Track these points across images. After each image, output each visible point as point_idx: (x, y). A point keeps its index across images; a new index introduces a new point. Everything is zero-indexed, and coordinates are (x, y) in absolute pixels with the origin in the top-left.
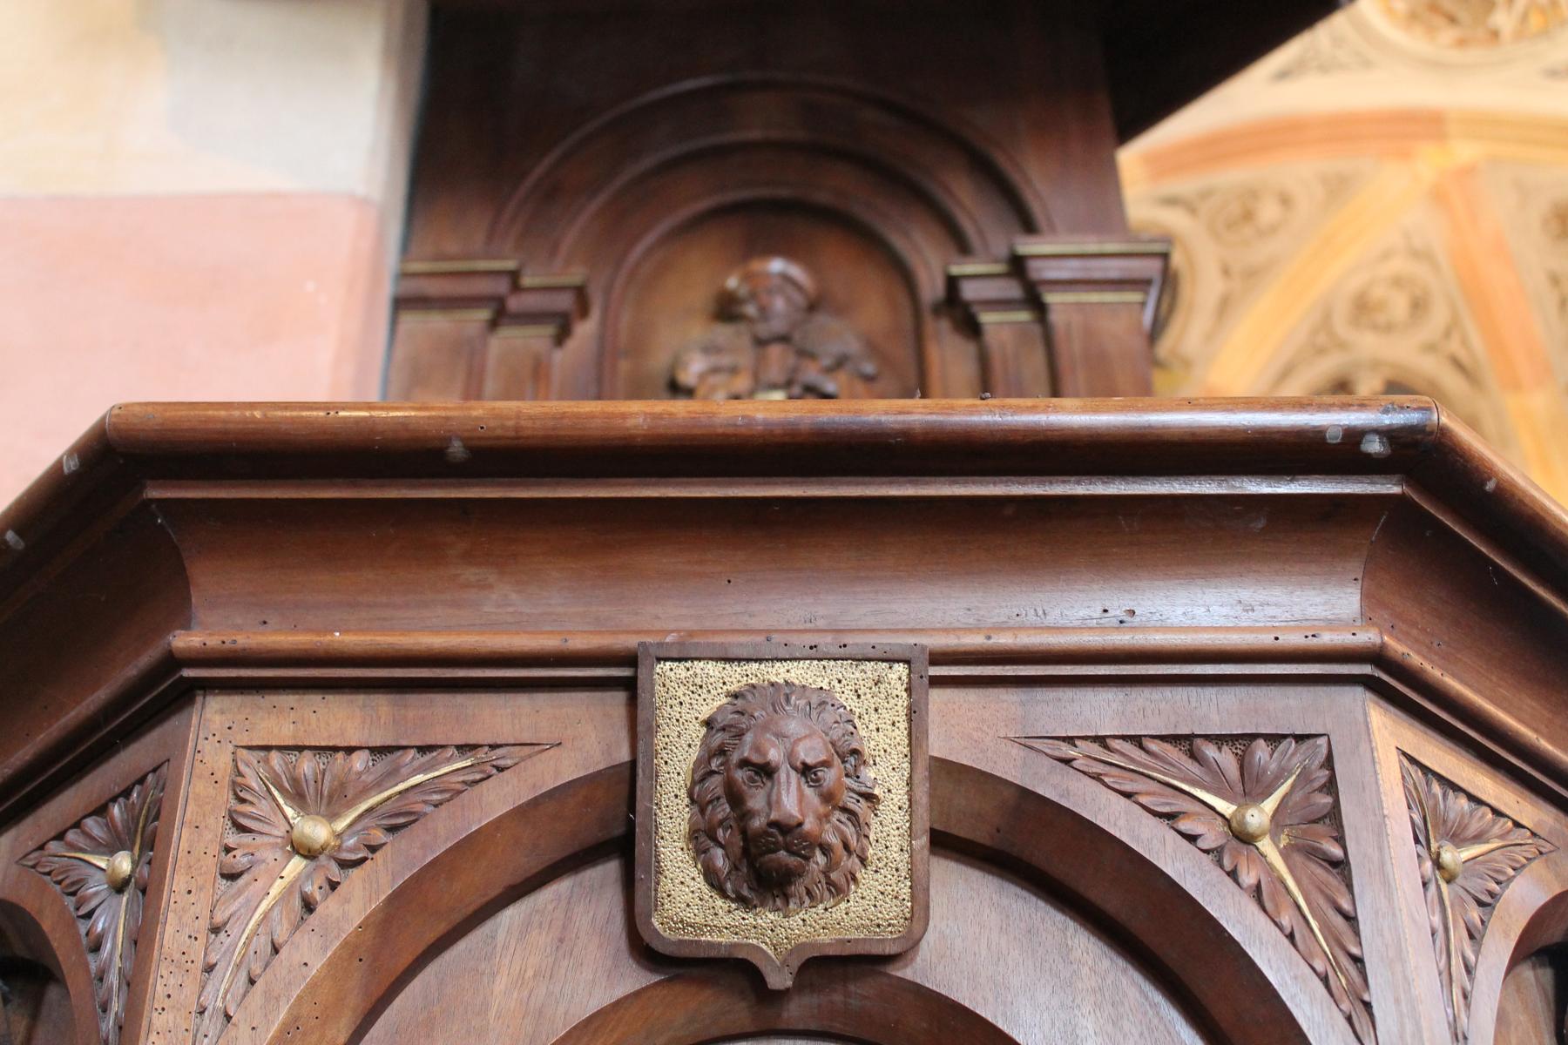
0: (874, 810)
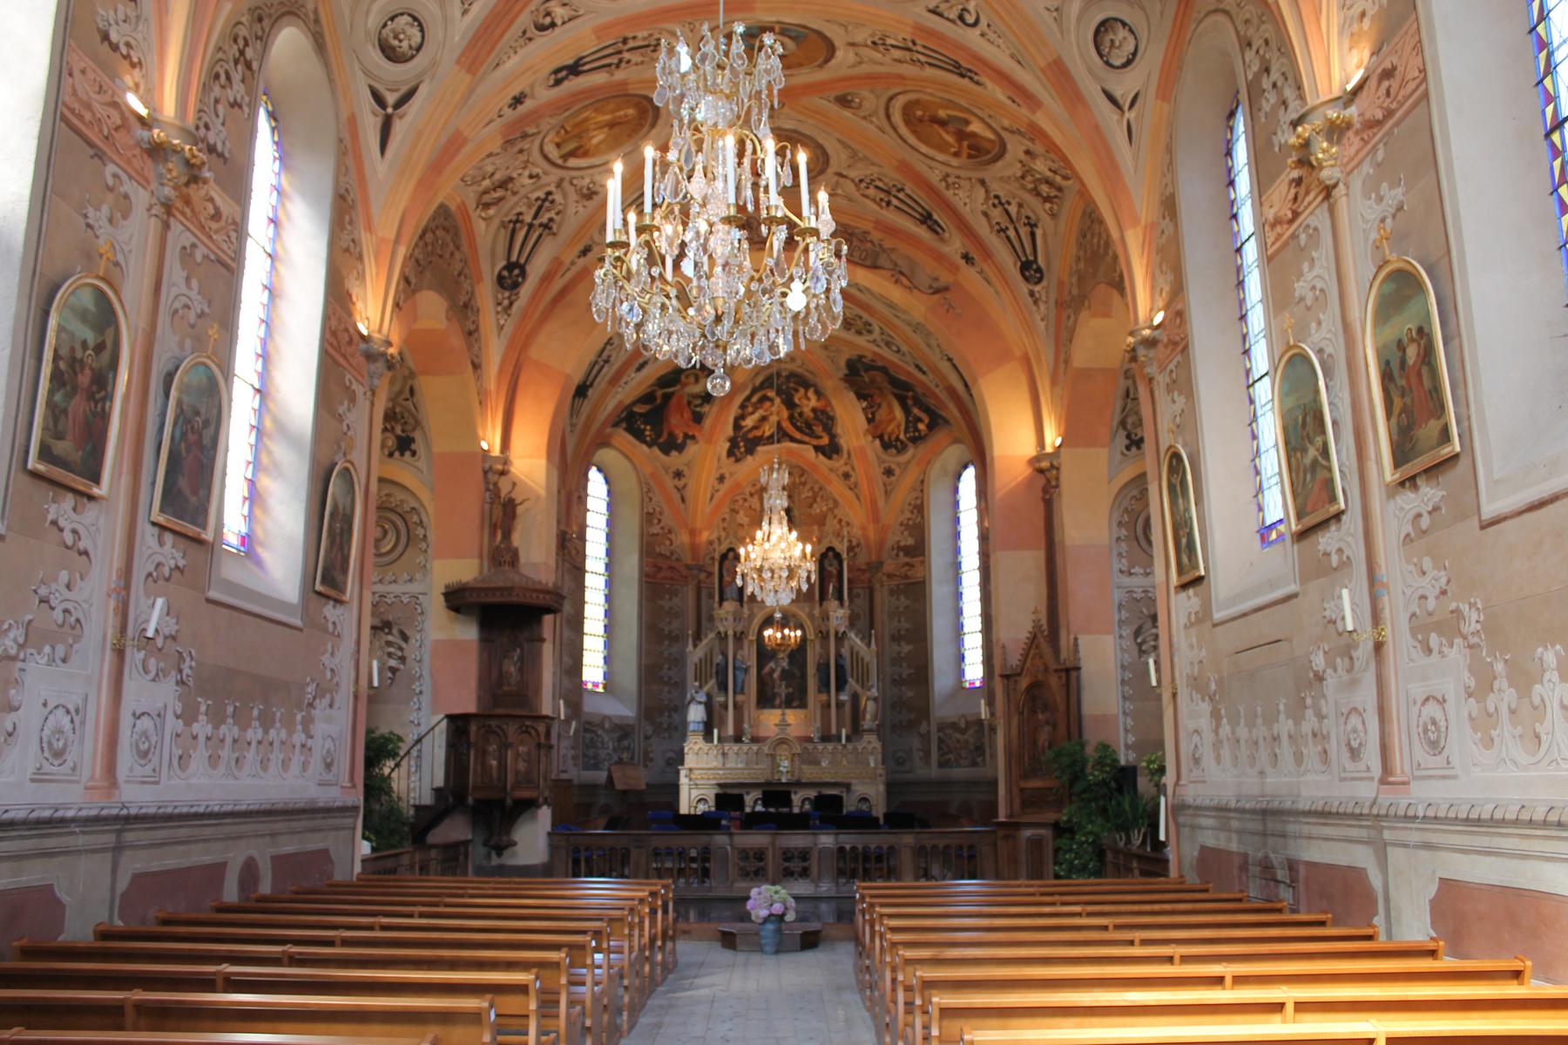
0: (741, 869)
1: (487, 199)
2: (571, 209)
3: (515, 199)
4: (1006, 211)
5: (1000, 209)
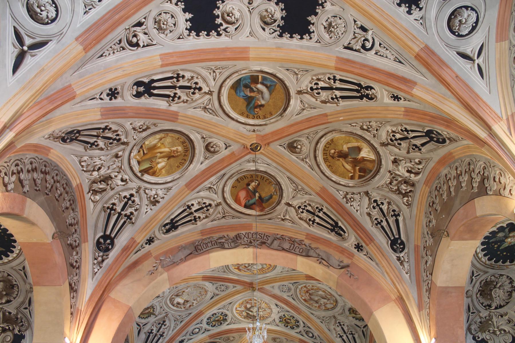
1: (95, 186)
2: (144, 209)
3: (112, 193)
4: (381, 209)
5: (377, 209)
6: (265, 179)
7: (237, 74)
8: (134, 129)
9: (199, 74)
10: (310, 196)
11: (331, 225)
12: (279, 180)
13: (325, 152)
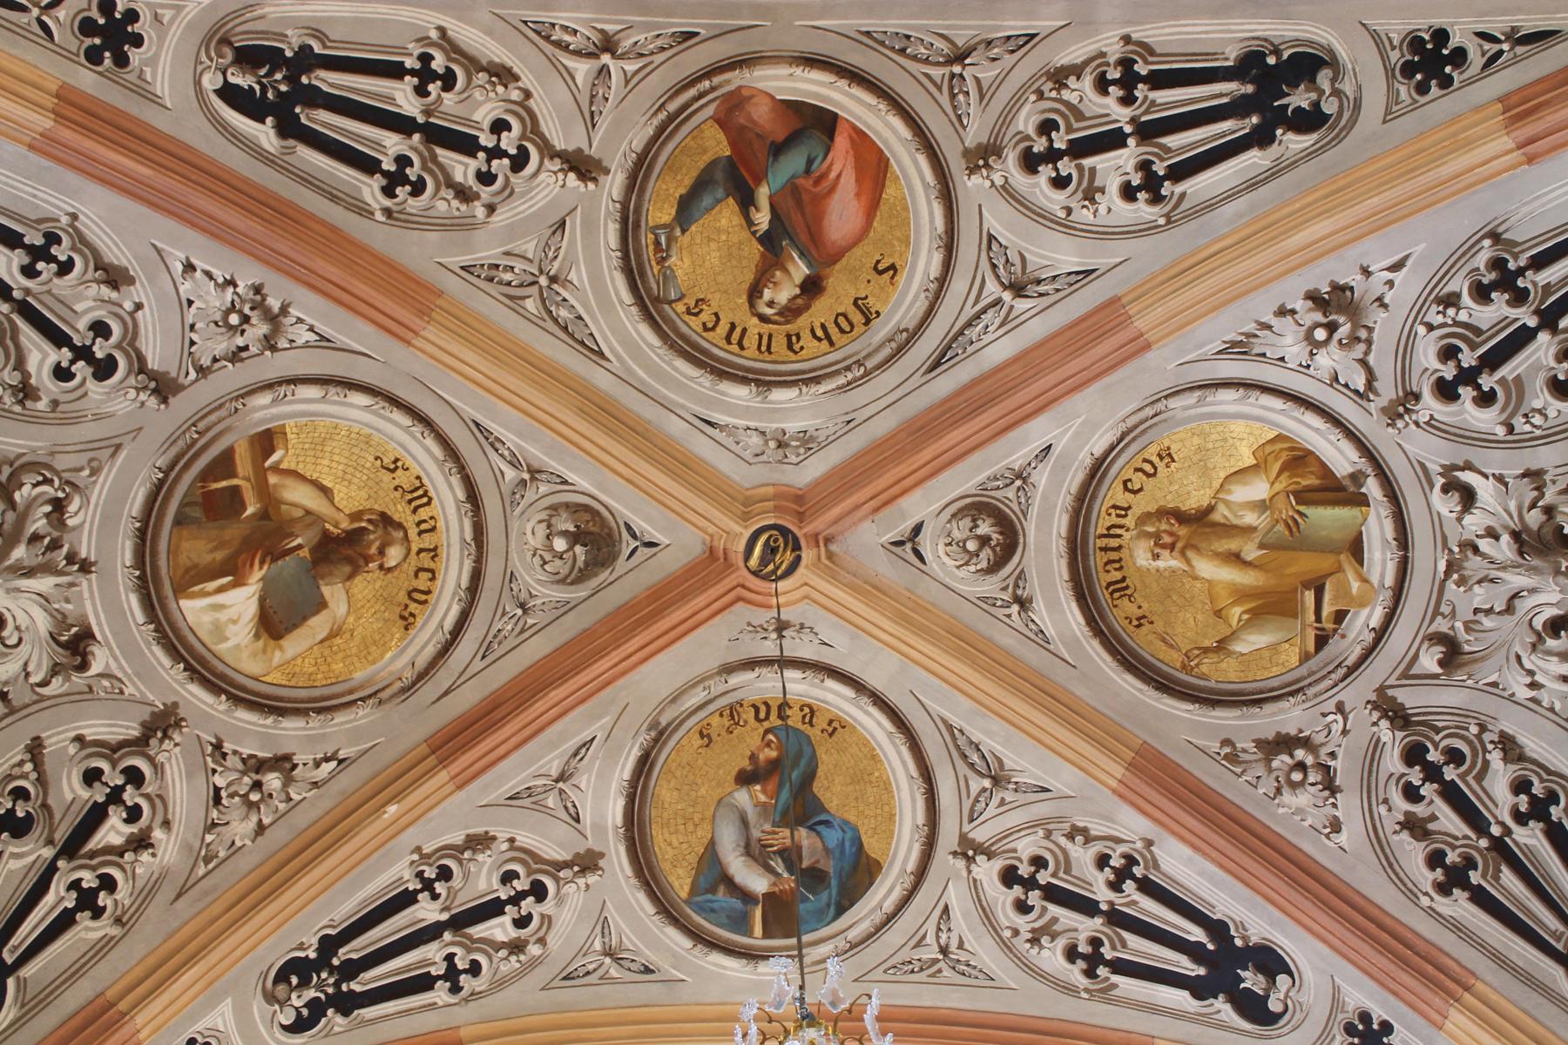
2: (1408, 287)
3: (1545, 457)
4: (58, 338)
6: (723, 329)
7: (853, 935)
8: (1330, 787)
9: (1006, 946)
10: (466, 259)
11: (352, 969)
12: (645, 330)
13: (428, 541)
